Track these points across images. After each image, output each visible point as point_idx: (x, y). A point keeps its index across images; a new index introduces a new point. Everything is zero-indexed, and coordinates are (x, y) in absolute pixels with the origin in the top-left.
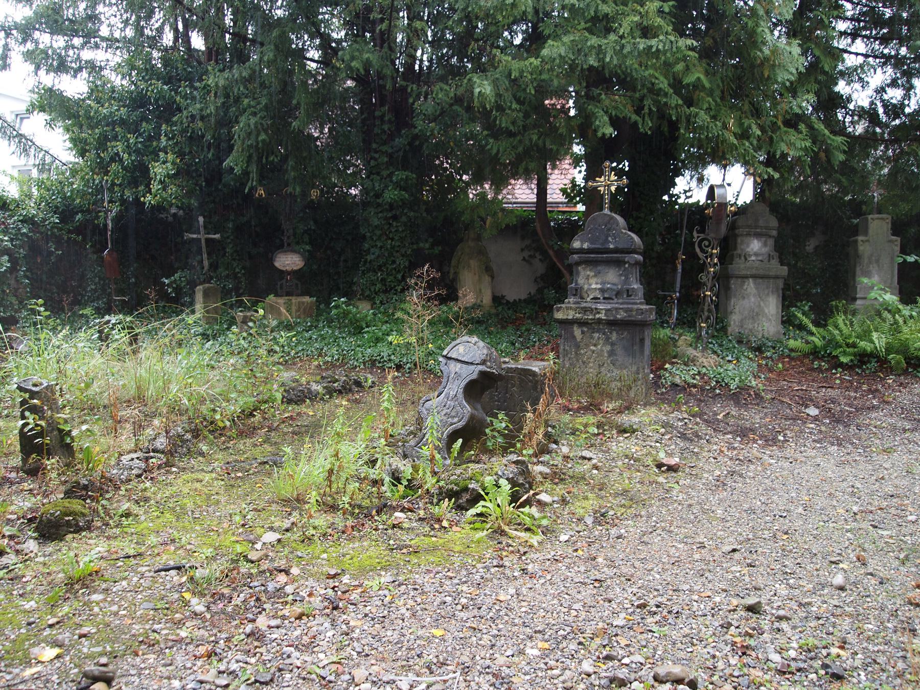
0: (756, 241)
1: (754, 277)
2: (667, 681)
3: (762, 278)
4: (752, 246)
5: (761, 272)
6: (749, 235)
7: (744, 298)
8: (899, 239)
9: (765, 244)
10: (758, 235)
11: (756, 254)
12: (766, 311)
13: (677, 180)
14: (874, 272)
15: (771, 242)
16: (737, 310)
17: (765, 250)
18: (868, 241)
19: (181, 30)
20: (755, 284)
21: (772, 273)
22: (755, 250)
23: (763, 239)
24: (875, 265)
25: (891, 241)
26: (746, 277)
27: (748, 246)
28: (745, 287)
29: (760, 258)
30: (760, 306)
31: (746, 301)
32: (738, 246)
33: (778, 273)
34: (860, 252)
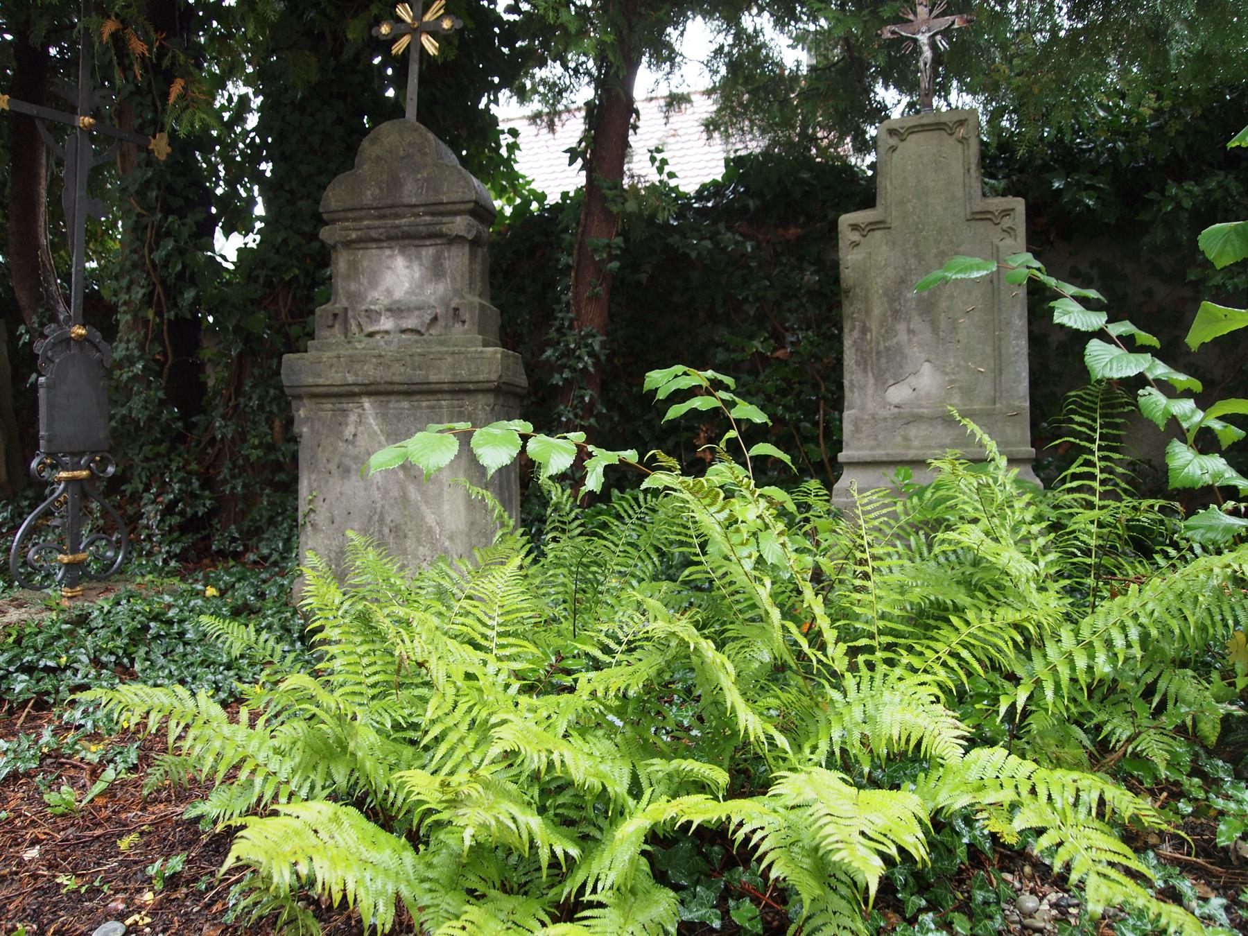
0: (400, 262)
1: (379, 391)
2: (193, 720)
3: (408, 394)
4: (388, 280)
5: (399, 374)
6: (366, 241)
7: (346, 472)
8: (1019, 204)
9: (437, 271)
10: (407, 239)
11: (396, 310)
12: (430, 519)
13: (169, 150)
14: (915, 352)
15: (457, 259)
16: (321, 518)
17: (435, 292)
18: (875, 226)
19: (786, 458)
20: (383, 417)
21: (441, 374)
22: (399, 294)
23: (428, 252)
24: (916, 323)
25: (981, 216)
26: (349, 394)
27: (373, 284)
28: (349, 431)
29: (410, 323)
30: (405, 497)
31: (354, 481)
32: (340, 284)
33: (464, 374)
34: (848, 275)
